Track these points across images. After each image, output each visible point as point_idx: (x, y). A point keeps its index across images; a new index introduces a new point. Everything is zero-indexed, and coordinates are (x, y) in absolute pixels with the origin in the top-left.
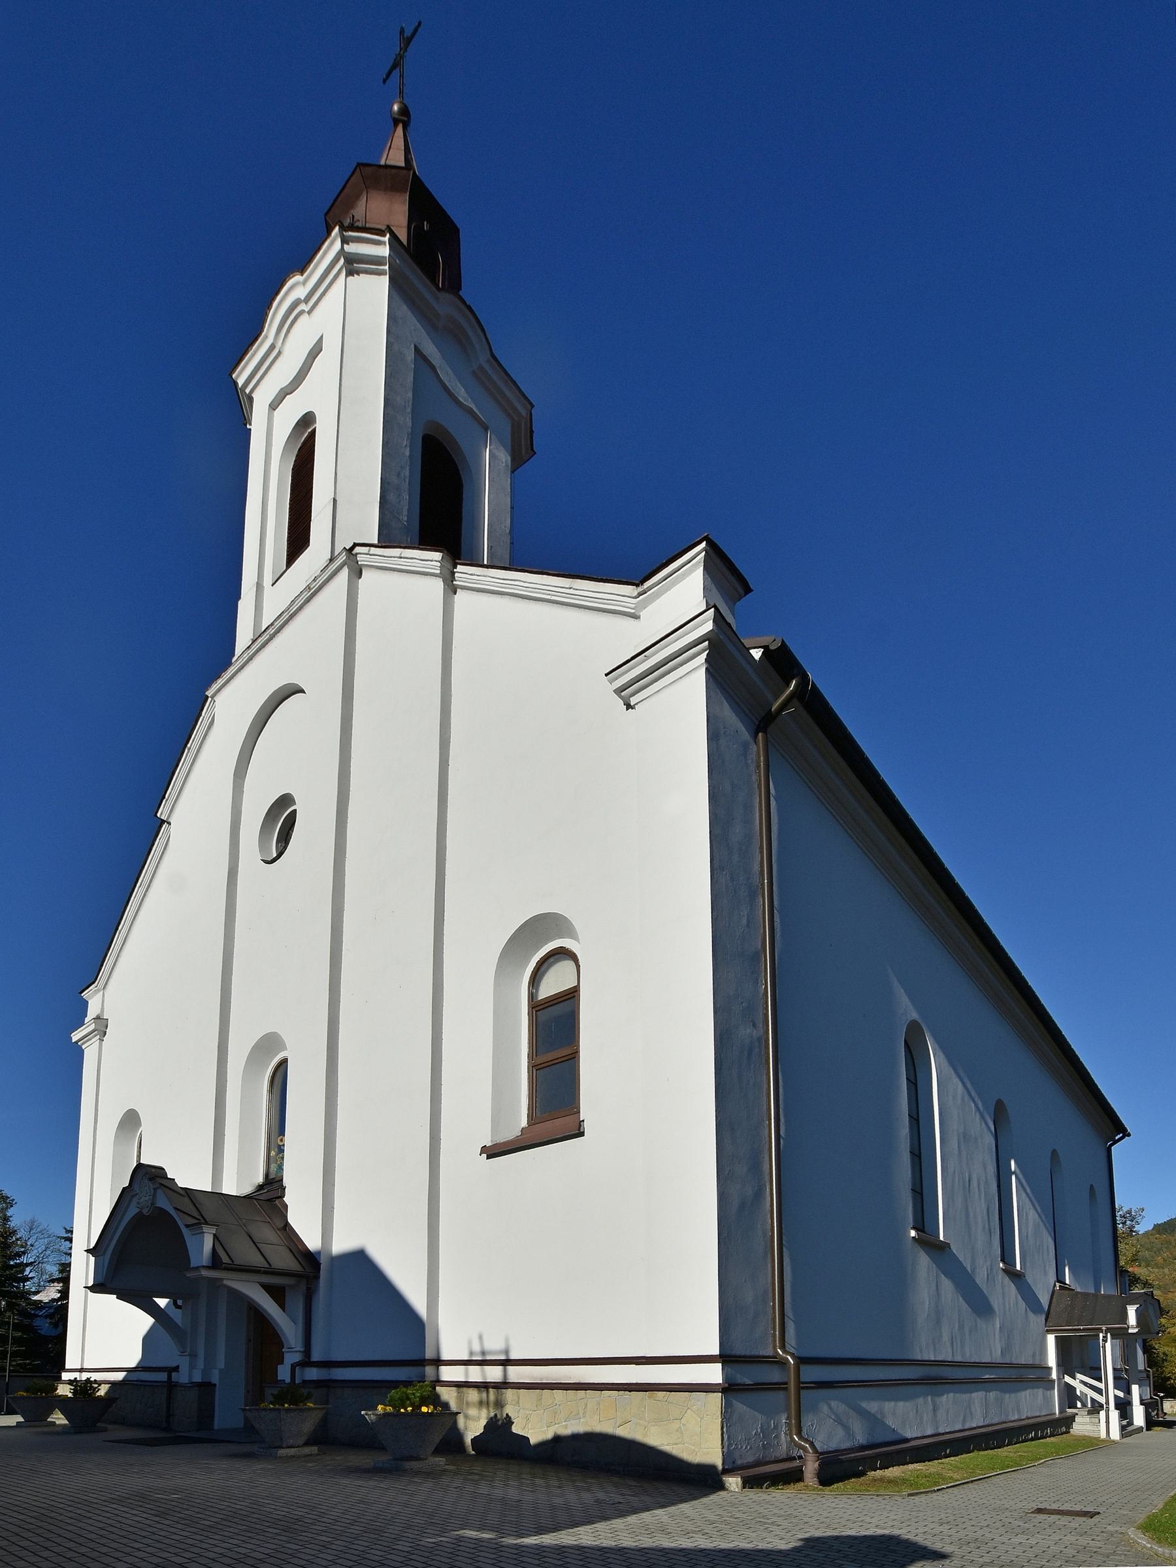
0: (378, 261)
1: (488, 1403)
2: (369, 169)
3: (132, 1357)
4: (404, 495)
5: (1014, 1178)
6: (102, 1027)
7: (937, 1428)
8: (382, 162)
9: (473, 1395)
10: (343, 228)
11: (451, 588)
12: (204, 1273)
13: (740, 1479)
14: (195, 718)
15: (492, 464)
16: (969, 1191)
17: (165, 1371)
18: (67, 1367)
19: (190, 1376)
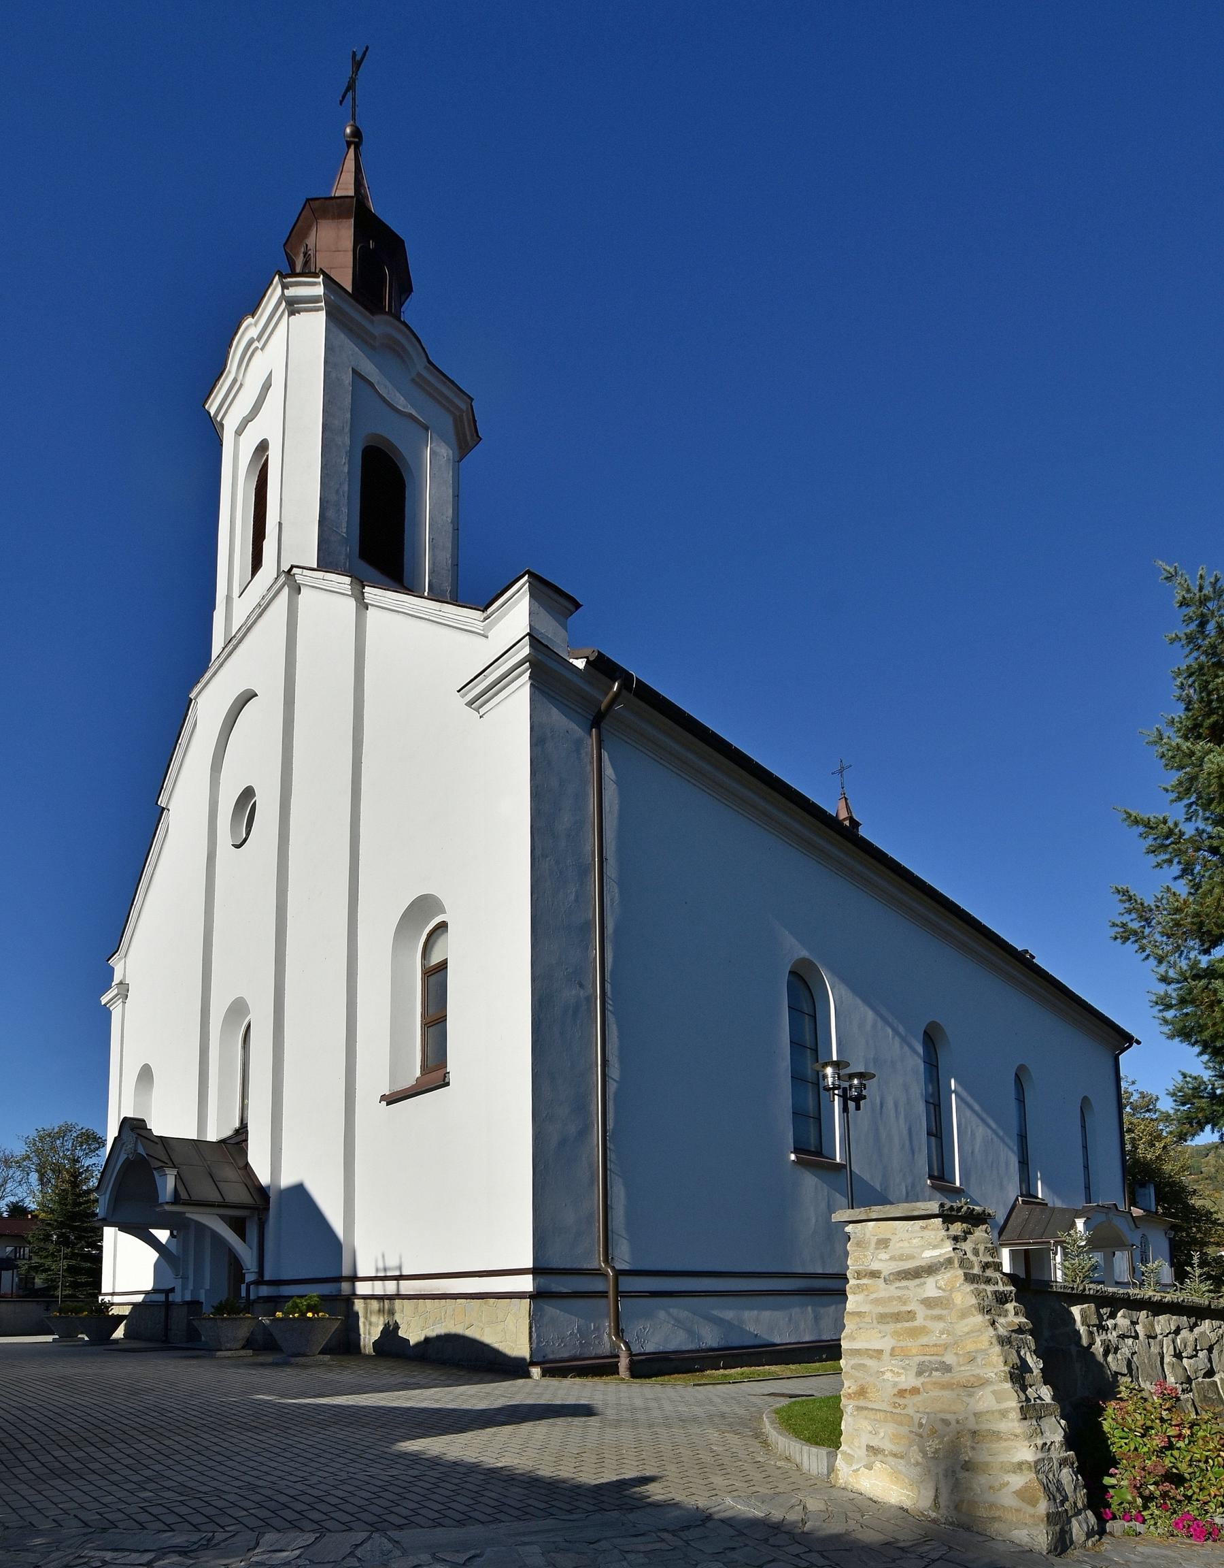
1: (383, 1311)
2: (317, 202)
3: (147, 1282)
4: (343, 509)
5: (953, 1096)
6: (124, 988)
7: (820, 1336)
8: (333, 195)
9: (375, 1305)
10: (282, 276)
11: (363, 605)
12: (167, 1208)
13: (539, 1369)
14: (183, 717)
15: (433, 462)
16: (881, 1113)
17: (163, 1293)
18: (103, 1292)
19: (183, 1295)
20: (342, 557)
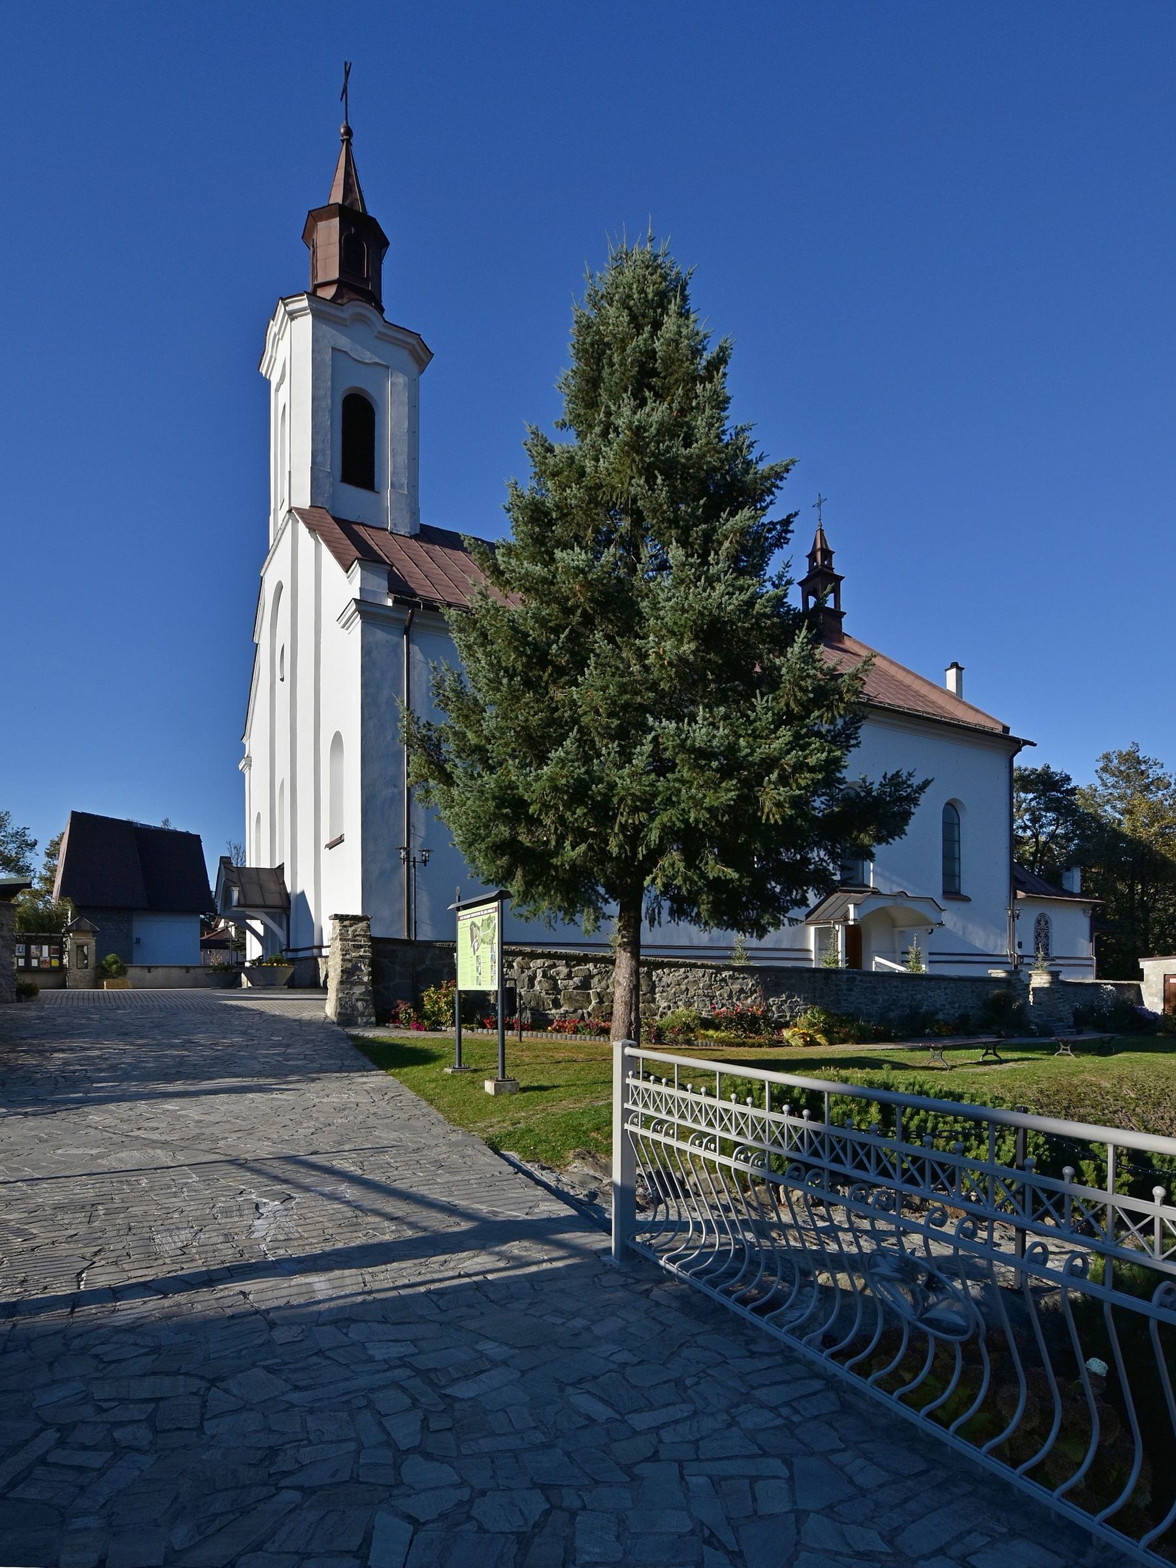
0: (304, 309)
20: (328, 486)
